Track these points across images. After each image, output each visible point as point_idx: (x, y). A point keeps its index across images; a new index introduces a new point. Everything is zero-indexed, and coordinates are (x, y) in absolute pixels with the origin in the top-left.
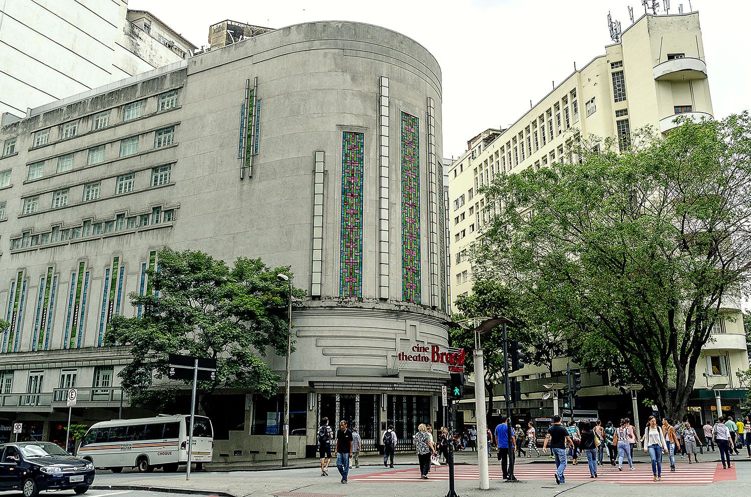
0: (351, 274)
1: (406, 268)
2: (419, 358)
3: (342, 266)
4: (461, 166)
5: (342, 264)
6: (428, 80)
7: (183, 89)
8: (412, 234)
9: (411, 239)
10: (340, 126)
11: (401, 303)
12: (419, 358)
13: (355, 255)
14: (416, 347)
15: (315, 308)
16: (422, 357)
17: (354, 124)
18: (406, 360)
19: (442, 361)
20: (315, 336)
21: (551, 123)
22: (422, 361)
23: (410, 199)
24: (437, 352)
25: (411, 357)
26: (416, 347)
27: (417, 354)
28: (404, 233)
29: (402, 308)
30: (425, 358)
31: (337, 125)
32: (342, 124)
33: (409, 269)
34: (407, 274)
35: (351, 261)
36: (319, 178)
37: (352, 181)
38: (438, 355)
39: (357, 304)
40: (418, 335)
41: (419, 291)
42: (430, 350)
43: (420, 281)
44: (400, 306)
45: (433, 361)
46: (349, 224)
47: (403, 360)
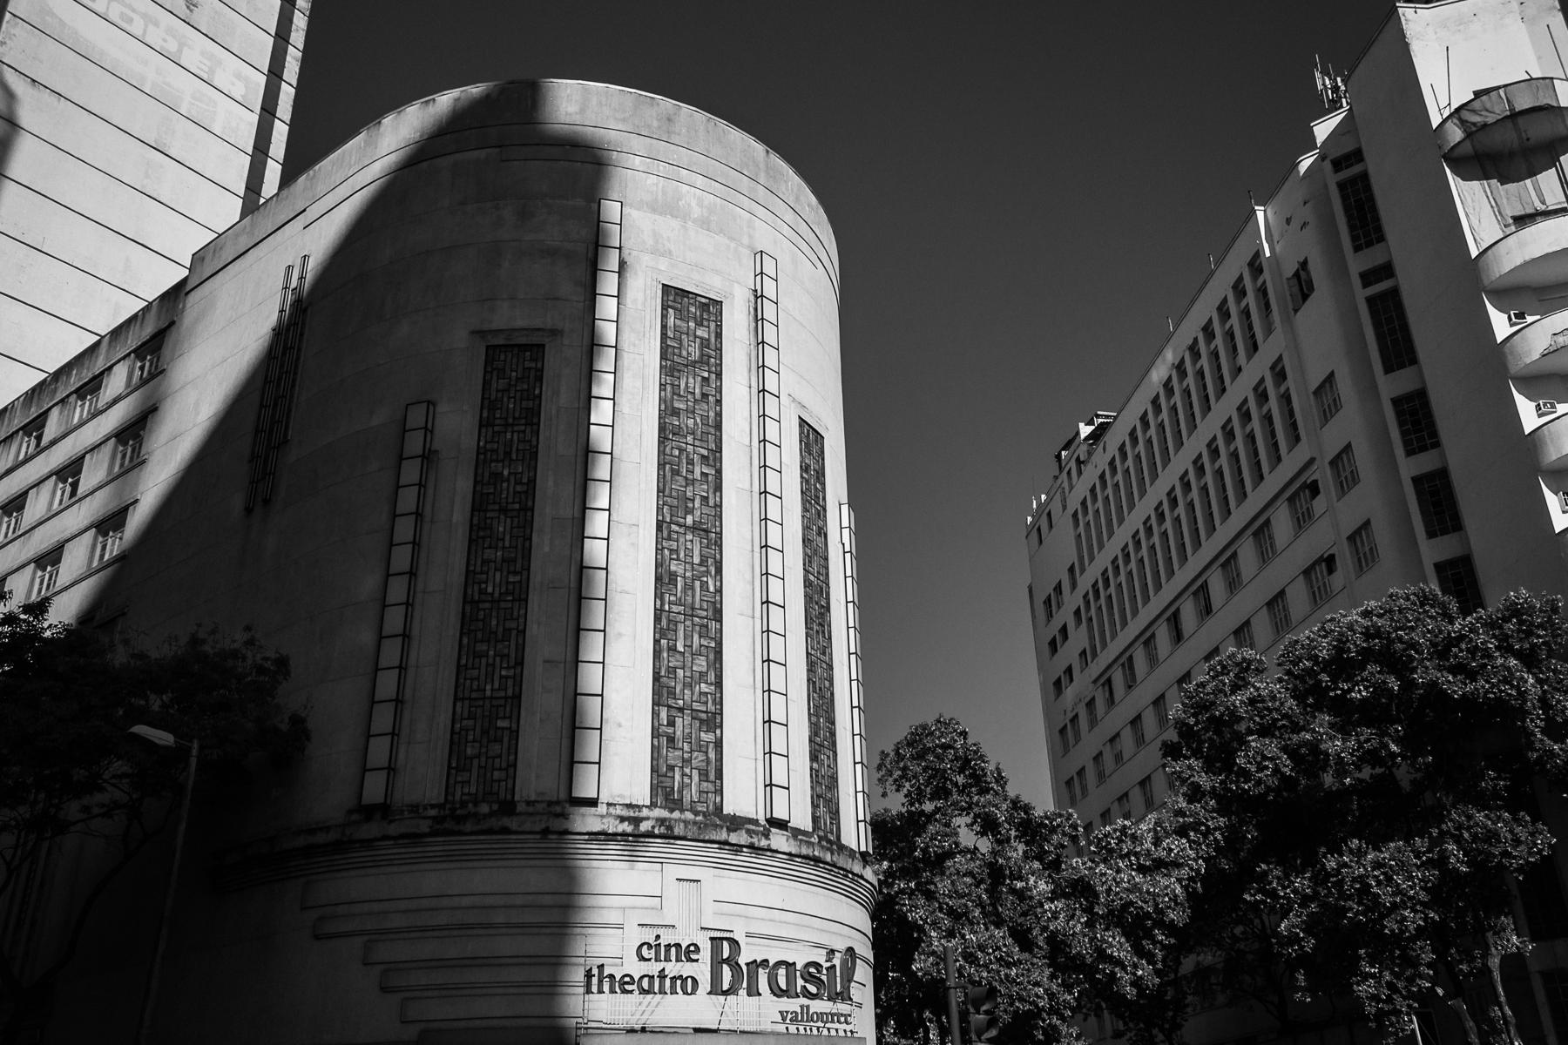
0: (485, 732)
1: (669, 707)
2: (662, 985)
3: (459, 709)
4: (1049, 514)
5: (459, 704)
6: (761, 211)
7: (174, 329)
8: (693, 609)
9: (688, 623)
10: (480, 333)
11: (645, 813)
12: (662, 985)
13: (501, 677)
14: (650, 946)
15: (368, 843)
16: (674, 979)
17: (520, 323)
18: (612, 991)
19: (753, 991)
20: (361, 933)
21: (1217, 357)
22: (674, 992)
23: (691, 511)
24: (732, 962)
25: (632, 981)
26: (650, 946)
27: (654, 968)
28: (662, 604)
29: (645, 826)
30: (684, 980)
31: (473, 332)
32: (486, 327)
33: (681, 710)
34: (671, 723)
35: (488, 693)
36: (411, 472)
37: (506, 473)
38: (735, 967)
39: (494, 823)
40: (709, 907)
41: (714, 775)
42: (705, 955)
43: (719, 744)
44: (636, 821)
45: (716, 989)
46: (490, 590)
47: (601, 991)
